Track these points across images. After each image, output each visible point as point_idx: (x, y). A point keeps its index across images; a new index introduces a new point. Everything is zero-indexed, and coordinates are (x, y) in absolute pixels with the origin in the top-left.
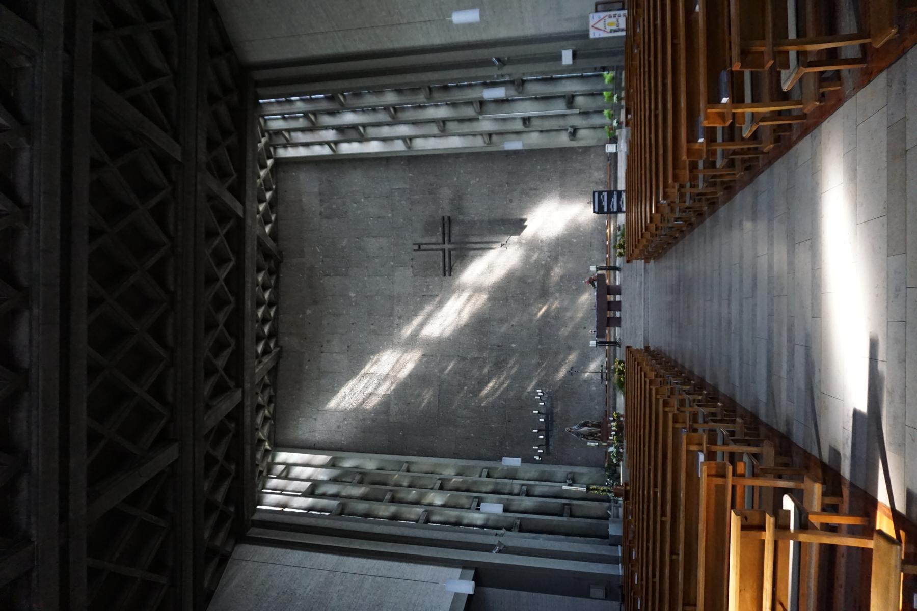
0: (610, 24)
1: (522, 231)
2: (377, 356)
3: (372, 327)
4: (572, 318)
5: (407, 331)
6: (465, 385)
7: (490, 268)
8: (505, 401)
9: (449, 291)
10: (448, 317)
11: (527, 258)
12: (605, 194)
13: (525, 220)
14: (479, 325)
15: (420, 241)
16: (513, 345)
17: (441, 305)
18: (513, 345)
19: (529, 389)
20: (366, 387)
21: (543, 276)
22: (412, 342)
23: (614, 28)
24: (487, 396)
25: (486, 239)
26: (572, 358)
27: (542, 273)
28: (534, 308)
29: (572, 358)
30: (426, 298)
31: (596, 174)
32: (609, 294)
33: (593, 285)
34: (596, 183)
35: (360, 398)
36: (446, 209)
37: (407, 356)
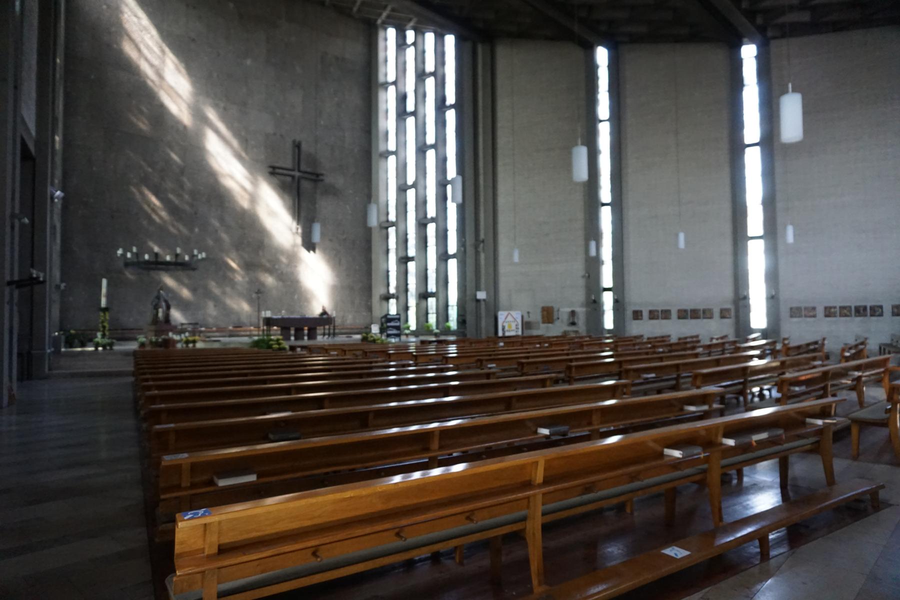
0: (510, 326)
2: (183, 71)
4: (224, 293)
5: (212, 115)
7: (272, 214)
11: (279, 251)
12: (398, 324)
13: (314, 251)
14: (216, 195)
19: (151, 244)
20: (148, 47)
23: (506, 328)
24: (142, 193)
26: (186, 293)
27: (268, 265)
28: (234, 254)
29: (186, 293)
30: (244, 141)
31: (350, 317)
34: (343, 317)
35: (136, 36)
36: (329, 179)
37: (184, 107)
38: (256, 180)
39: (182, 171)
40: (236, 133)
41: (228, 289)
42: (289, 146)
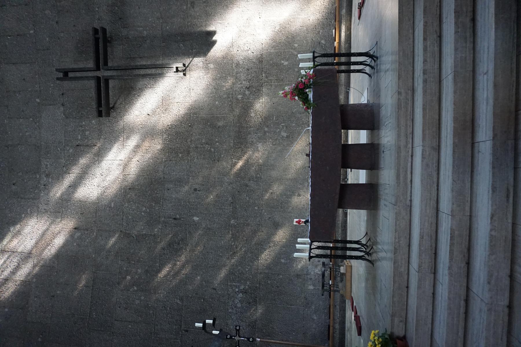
1: (208, 50)
3: (14, 187)
5: (58, 191)
6: (128, 273)
7: (165, 104)
8: (181, 299)
9: (112, 137)
10: (111, 170)
11: (216, 92)
13: (213, 33)
14: (146, 189)
15: (69, 64)
16: (196, 219)
17: (99, 156)
18: (196, 219)
21: (240, 117)
22: (62, 208)
25: (160, 62)
27: (237, 111)
30: (80, 148)
33: (305, 99)
37: (56, 228)
38: (123, 130)
40: (73, 160)
41: (274, 174)
42: (58, 82)
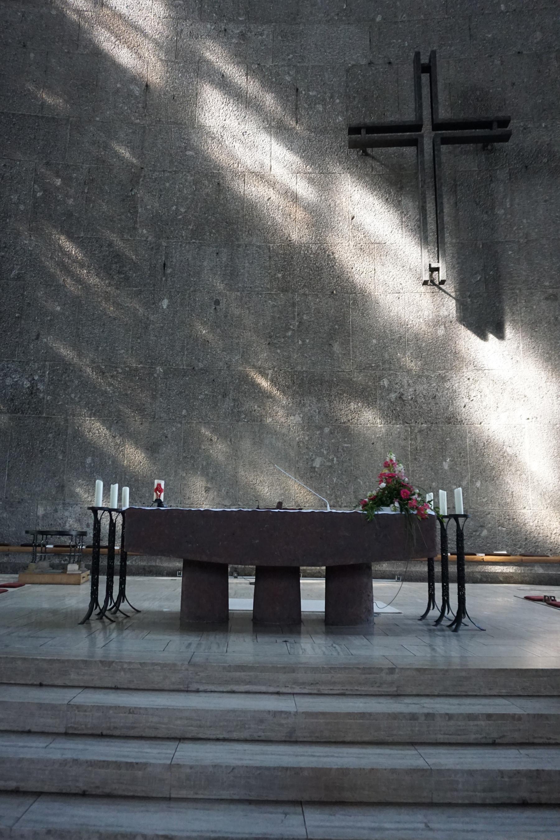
1: (470, 326)
5: (215, 55)
6: (67, 180)
7: (372, 247)
9: (312, 154)
10: (253, 150)
11: (394, 339)
13: (500, 335)
14: (219, 214)
16: (165, 303)
17: (278, 129)
18: (165, 303)
22: (184, 61)
25: (448, 239)
27: (359, 378)
30: (293, 96)
32: (263, 575)
33: (381, 500)
37: (148, 51)
39: (135, 179)
